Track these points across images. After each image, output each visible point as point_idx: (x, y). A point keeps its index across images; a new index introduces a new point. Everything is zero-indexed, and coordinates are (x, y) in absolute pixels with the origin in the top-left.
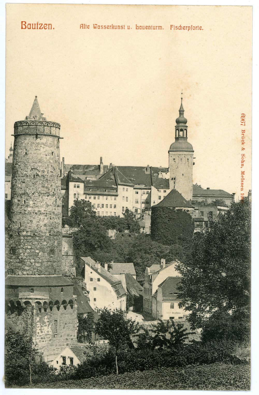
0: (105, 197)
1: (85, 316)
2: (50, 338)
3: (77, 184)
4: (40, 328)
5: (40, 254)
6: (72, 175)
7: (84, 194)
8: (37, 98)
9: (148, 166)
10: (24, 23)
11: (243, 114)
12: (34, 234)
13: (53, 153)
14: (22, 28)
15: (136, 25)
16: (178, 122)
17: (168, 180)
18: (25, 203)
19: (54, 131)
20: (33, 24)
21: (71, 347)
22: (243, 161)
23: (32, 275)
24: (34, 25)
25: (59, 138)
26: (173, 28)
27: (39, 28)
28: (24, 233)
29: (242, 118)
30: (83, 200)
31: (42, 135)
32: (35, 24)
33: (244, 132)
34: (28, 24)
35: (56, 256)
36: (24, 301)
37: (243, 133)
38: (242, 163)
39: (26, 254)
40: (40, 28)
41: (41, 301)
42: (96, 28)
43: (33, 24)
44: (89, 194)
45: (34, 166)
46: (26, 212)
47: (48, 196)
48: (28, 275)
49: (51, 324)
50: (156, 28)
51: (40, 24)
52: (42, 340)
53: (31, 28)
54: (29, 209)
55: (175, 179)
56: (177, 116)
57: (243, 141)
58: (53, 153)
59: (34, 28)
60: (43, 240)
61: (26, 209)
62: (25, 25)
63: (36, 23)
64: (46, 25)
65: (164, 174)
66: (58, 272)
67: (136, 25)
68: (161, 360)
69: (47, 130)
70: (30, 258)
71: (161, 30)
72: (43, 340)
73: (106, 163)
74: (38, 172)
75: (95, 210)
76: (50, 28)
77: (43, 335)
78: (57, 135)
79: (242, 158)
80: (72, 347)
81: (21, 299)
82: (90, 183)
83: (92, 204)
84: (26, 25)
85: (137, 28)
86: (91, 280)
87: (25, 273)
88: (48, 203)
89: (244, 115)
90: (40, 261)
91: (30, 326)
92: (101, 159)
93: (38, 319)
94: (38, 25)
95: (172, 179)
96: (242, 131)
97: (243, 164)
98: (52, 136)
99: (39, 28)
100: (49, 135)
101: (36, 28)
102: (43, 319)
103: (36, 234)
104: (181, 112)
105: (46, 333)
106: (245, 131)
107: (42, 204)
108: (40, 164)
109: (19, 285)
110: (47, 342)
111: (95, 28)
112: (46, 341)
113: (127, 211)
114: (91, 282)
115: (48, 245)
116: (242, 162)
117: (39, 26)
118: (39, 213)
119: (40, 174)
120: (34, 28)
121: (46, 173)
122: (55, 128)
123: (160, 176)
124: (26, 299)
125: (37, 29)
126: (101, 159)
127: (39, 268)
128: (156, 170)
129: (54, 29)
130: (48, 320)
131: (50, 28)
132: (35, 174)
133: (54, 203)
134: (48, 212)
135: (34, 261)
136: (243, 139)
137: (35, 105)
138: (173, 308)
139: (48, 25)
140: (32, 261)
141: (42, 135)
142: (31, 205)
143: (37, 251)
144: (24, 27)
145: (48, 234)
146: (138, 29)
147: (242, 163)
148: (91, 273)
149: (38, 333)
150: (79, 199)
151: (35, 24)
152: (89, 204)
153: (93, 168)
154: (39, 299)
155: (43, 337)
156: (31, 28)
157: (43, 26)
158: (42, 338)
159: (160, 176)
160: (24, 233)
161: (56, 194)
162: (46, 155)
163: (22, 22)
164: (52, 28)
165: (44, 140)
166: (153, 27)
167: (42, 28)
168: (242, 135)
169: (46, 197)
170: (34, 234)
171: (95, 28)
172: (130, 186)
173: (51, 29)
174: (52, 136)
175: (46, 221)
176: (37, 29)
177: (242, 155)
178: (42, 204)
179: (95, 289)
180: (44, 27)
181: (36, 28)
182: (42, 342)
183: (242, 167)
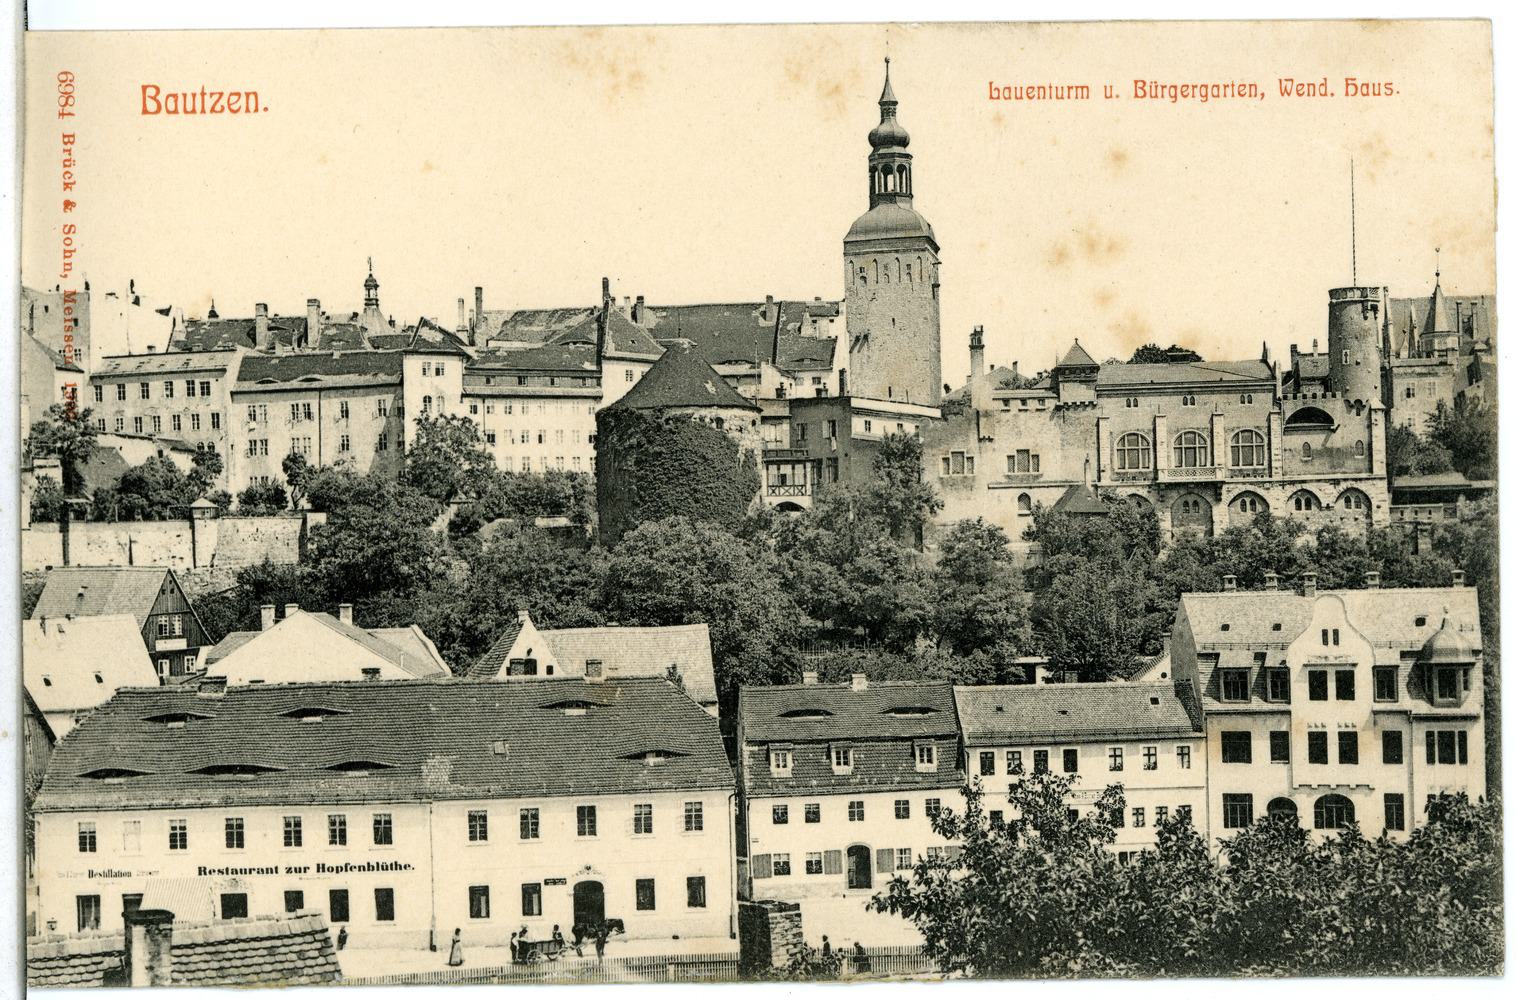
7: (464, 396)
10: (151, 92)
11: (66, 73)
14: (145, 111)
15: (991, 83)
20: (185, 95)
22: (70, 251)
24: (189, 99)
26: (68, 109)
27: (208, 108)
29: (62, 89)
32: (194, 95)
33: (72, 143)
34: (167, 98)
37: (68, 147)
38: (67, 261)
40: (213, 110)
42: (1289, 94)
43: (185, 95)
44: (483, 397)
50: (1159, 95)
51: (212, 94)
55: (866, 337)
59: (189, 108)
62: (154, 98)
63: (199, 92)
64: (236, 98)
67: (991, 83)
76: (252, 106)
79: (68, 241)
82: (497, 359)
84: (161, 98)
85: (995, 94)
89: (70, 77)
94: (207, 97)
96: (64, 136)
97: (70, 264)
99: (208, 108)
101: (198, 108)
106: (73, 136)
111: (1285, 92)
116: (65, 257)
120: (189, 108)
125: (203, 111)
129: (266, 109)
131: (252, 106)
136: (67, 169)
138: (184, 846)
139: (243, 98)
144: (151, 106)
146: (998, 98)
147: (67, 261)
151: (194, 95)
157: (224, 101)
163: (144, 88)
164: (261, 108)
166: (1054, 90)
167: (223, 108)
171: (1285, 92)
173: (256, 110)
176: (203, 111)
177: (67, 230)
180: (229, 105)
181: (198, 108)
183: (66, 276)
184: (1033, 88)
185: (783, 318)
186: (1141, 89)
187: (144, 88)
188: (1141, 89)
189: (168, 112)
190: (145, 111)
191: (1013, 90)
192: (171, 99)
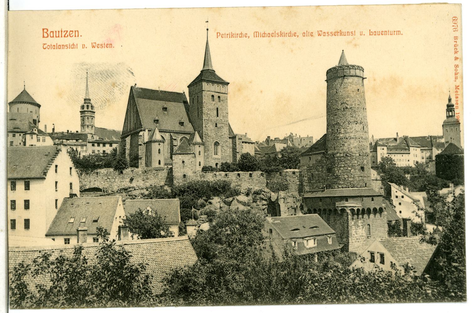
0: (401, 155)
1: (394, 222)
2: (365, 239)
3: (382, 147)
4: (355, 231)
5: (352, 171)
6: (379, 142)
8: (344, 51)
9: (429, 136)
12: (346, 155)
13: (358, 90)
14: (44, 37)
15: (370, 30)
16: (448, 106)
17: (444, 143)
18: (337, 131)
19: (358, 72)
20: (56, 32)
21: (380, 240)
22: (457, 73)
23: (346, 188)
24: (57, 33)
25: (363, 79)
27: (63, 36)
28: (338, 155)
29: (454, 22)
30: (387, 157)
31: (348, 76)
32: (59, 32)
33: (457, 39)
35: (366, 172)
36: (340, 208)
37: (456, 40)
38: (456, 76)
39: (340, 171)
40: (65, 36)
41: (354, 208)
42: (95, 47)
44: (390, 154)
45: (343, 101)
46: (339, 138)
47: (356, 124)
48: (343, 188)
49: (364, 227)
51: (64, 31)
52: (357, 241)
53: (377, 34)
54: (341, 135)
56: (447, 102)
57: (456, 49)
58: (358, 90)
59: (57, 36)
60: (354, 160)
61: (338, 136)
62: (46, 33)
65: (440, 139)
66: (368, 185)
67: (370, 30)
68: (24, 292)
69: (352, 72)
70: (344, 174)
71: (348, 36)
72: (358, 240)
73: (401, 135)
74: (346, 106)
75: (395, 163)
76: (77, 35)
77: (358, 236)
78: (361, 76)
79: (456, 70)
80: (382, 240)
81: (337, 207)
83: (393, 159)
84: (49, 33)
85: (371, 34)
86: (397, 197)
87: (340, 187)
88: (357, 129)
89: (456, 18)
90: (353, 176)
91: (346, 229)
92: (397, 133)
93: (353, 223)
94: (63, 32)
95: (446, 142)
98: (357, 76)
99: (63, 36)
100: (355, 76)
101: (60, 36)
102: (358, 224)
103: (348, 155)
104: (450, 100)
105: (360, 235)
107: (351, 131)
108: (348, 99)
109: (336, 196)
110: (362, 242)
111: (93, 47)
112: (361, 242)
113: (417, 162)
114: (397, 199)
115: (359, 163)
116: (455, 75)
117: (63, 34)
118: (350, 138)
119: (348, 107)
120: (57, 36)
121: (354, 106)
122: (359, 70)
123: (438, 141)
124: (342, 207)
125: (62, 37)
126: (397, 133)
127: (352, 182)
128: (435, 138)
130: (362, 224)
131: (77, 35)
132: (344, 107)
133: (362, 129)
134: (357, 137)
135: (347, 176)
136: (456, 47)
137: (342, 57)
140: (346, 176)
141: (348, 76)
142: (343, 132)
143: (349, 169)
144: (46, 35)
145: (358, 155)
146: (372, 35)
147: (456, 76)
148: (396, 192)
149: (354, 235)
150: (384, 157)
151: (59, 32)
152: (391, 160)
153: (392, 139)
154: (353, 207)
155: (357, 238)
156: (377, 34)
158: (357, 239)
159: (438, 141)
160: (338, 155)
161: (363, 122)
162: (353, 92)
163: (43, 29)
164: (79, 36)
165: (350, 80)
166: (389, 32)
167: (68, 35)
168: (455, 43)
169: (355, 125)
170: (346, 155)
171: (93, 47)
172: (418, 147)
173: (78, 36)
174: (357, 76)
175: (356, 144)
176: (62, 37)
177: (456, 66)
178: (351, 131)
179: (400, 204)
181: (60, 36)
182: (357, 243)
184: (383, 31)
185: (432, 139)
186: (371, 33)
187: (43, 29)
188: (371, 33)
189: (51, 37)
190: (44, 37)
191: (377, 32)
192: (52, 33)
